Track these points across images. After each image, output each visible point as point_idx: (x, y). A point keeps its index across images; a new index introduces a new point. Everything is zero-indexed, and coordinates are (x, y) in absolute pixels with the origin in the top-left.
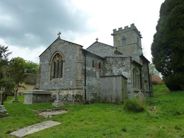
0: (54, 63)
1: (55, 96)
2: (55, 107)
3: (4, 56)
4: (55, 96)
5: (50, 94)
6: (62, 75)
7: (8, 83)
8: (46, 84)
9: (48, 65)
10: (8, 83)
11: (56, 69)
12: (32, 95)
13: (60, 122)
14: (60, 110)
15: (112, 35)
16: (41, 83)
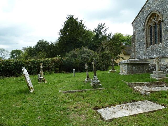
0: (149, 27)
1: (154, 66)
2: (155, 80)
3: (103, 32)
4: (154, 66)
5: (147, 64)
7: (108, 55)
9: (142, 32)
10: (108, 55)
11: (153, 33)
12: (126, 65)
13: (163, 105)
14: (162, 83)
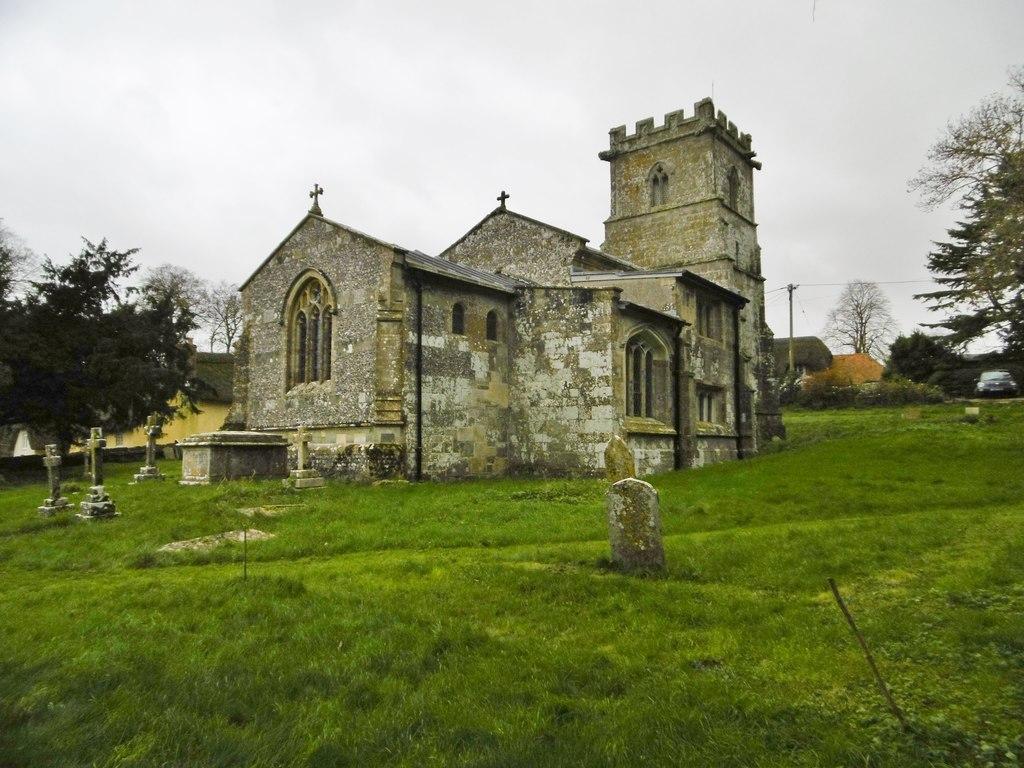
6: (329, 371)
8: (270, 405)
12: (208, 451)
15: (604, 156)
16: (250, 403)
